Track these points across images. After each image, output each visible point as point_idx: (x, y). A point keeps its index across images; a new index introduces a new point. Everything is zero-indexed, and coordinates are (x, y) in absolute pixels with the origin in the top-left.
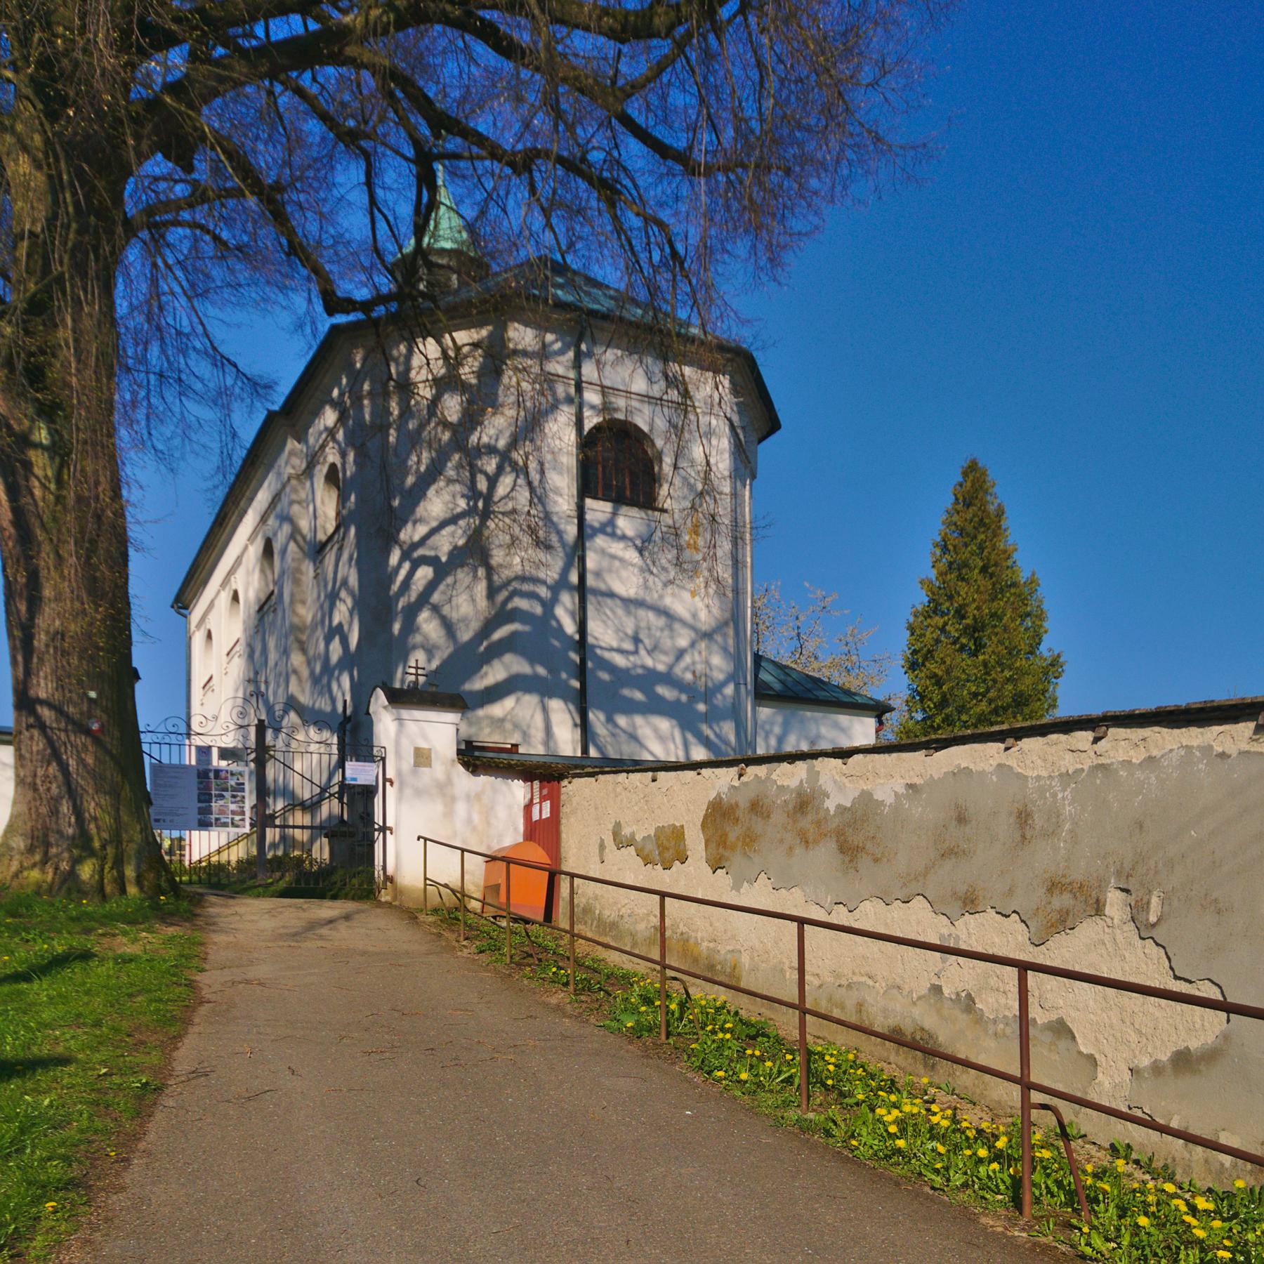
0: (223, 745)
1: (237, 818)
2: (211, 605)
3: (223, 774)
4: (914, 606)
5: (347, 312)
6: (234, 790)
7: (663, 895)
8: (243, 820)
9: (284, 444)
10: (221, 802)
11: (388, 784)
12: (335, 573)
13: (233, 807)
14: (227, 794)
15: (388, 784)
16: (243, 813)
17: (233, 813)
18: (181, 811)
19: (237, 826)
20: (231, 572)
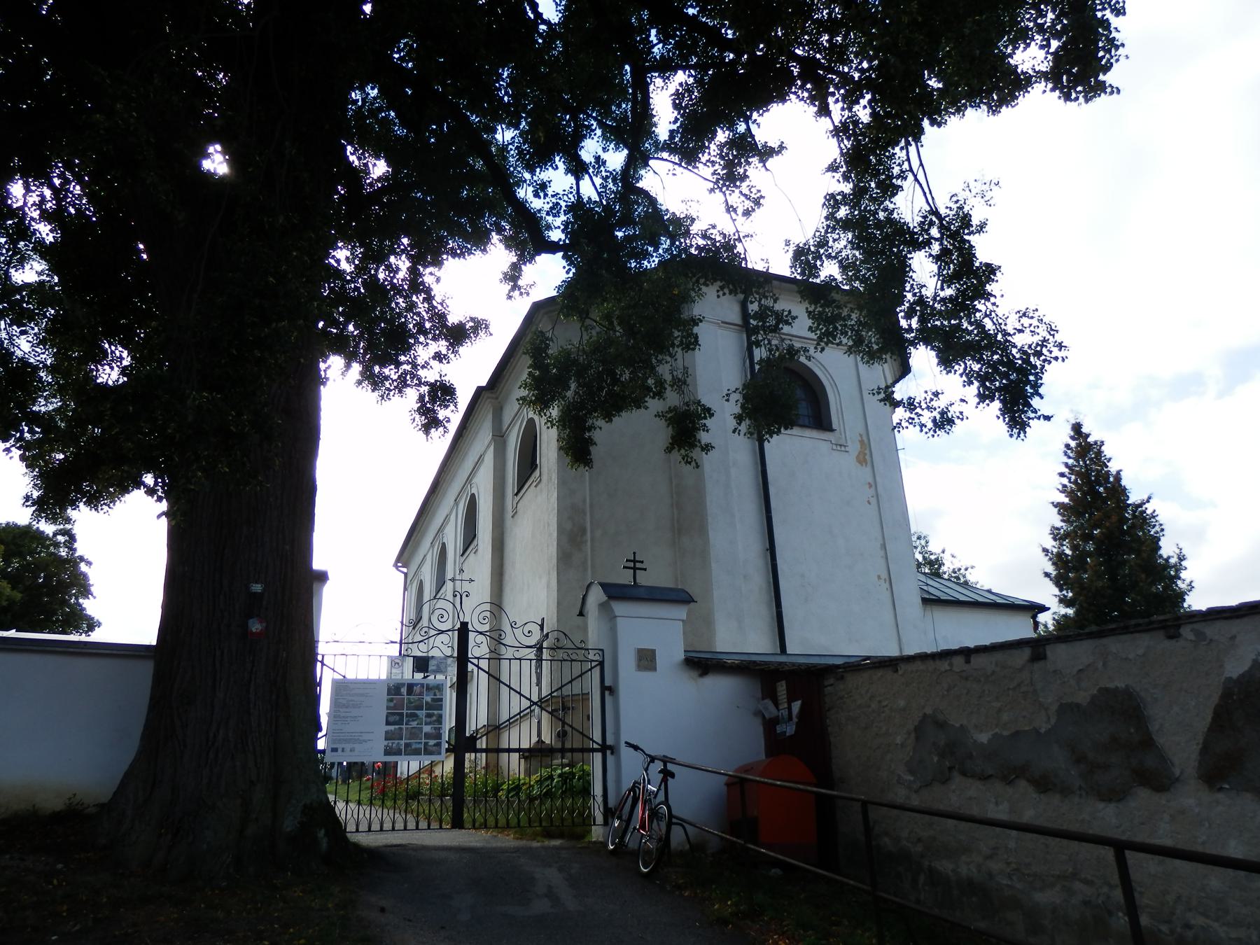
0: (420, 654)
1: (432, 742)
2: (447, 518)
3: (417, 689)
4: (1045, 550)
5: (329, 715)
6: (429, 707)
7: (1120, 847)
8: (439, 745)
9: (714, 134)
10: (414, 724)
11: (607, 693)
12: (497, 605)
13: (427, 729)
14: (422, 713)
15: (607, 693)
16: (439, 736)
17: (428, 736)
18: (365, 737)
19: (431, 753)
20: (441, 530)
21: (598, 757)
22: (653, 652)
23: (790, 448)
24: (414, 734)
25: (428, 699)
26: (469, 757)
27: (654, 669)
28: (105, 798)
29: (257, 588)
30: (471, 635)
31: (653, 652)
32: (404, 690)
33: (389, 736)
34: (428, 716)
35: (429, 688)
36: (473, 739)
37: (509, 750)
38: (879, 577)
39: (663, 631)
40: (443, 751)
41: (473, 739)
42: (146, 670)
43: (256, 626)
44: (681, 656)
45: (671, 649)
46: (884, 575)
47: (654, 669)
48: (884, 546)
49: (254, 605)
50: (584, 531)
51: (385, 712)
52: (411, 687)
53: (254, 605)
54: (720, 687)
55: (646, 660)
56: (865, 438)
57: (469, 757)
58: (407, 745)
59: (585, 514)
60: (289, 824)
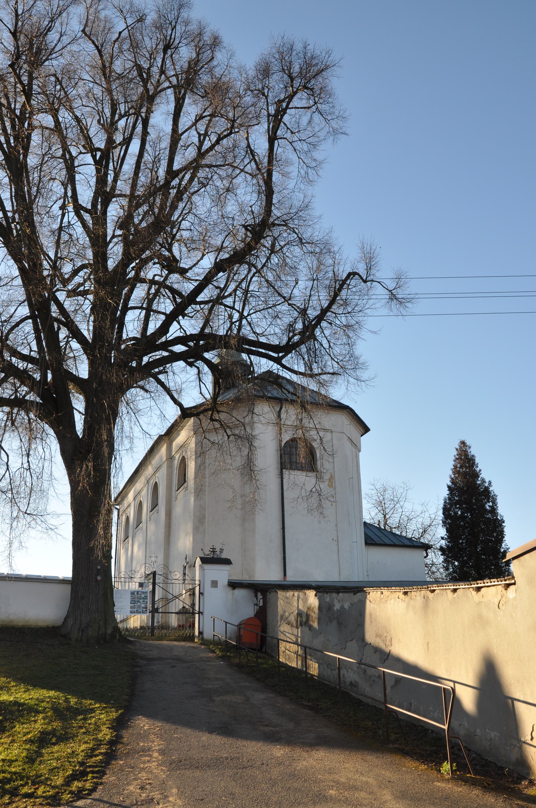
1: (144, 610)
3: (140, 593)
6: (143, 598)
8: (146, 610)
10: (139, 604)
13: (143, 605)
14: (141, 601)
17: (143, 608)
18: (124, 608)
21: (197, 616)
22: (217, 581)
23: (300, 480)
24: (139, 607)
25: (143, 596)
26: (156, 614)
27: (217, 587)
28: (60, 623)
29: (99, 567)
30: (157, 576)
31: (217, 581)
32: (136, 593)
33: (131, 607)
34: (143, 601)
35: (143, 593)
36: (157, 609)
37: (172, 613)
38: (333, 539)
39: (221, 574)
40: (148, 611)
41: (157, 609)
42: (68, 588)
43: (99, 578)
44: (226, 583)
45: (223, 581)
46: (335, 539)
47: (217, 587)
48: (336, 525)
49: (98, 572)
50: (204, 517)
51: (130, 600)
52: (138, 592)
53: (98, 572)
54: (240, 593)
55: (214, 584)
56: (333, 474)
57: (156, 614)
58: (137, 610)
59: (205, 509)
60: (109, 632)
